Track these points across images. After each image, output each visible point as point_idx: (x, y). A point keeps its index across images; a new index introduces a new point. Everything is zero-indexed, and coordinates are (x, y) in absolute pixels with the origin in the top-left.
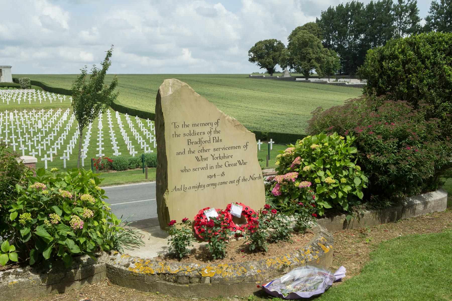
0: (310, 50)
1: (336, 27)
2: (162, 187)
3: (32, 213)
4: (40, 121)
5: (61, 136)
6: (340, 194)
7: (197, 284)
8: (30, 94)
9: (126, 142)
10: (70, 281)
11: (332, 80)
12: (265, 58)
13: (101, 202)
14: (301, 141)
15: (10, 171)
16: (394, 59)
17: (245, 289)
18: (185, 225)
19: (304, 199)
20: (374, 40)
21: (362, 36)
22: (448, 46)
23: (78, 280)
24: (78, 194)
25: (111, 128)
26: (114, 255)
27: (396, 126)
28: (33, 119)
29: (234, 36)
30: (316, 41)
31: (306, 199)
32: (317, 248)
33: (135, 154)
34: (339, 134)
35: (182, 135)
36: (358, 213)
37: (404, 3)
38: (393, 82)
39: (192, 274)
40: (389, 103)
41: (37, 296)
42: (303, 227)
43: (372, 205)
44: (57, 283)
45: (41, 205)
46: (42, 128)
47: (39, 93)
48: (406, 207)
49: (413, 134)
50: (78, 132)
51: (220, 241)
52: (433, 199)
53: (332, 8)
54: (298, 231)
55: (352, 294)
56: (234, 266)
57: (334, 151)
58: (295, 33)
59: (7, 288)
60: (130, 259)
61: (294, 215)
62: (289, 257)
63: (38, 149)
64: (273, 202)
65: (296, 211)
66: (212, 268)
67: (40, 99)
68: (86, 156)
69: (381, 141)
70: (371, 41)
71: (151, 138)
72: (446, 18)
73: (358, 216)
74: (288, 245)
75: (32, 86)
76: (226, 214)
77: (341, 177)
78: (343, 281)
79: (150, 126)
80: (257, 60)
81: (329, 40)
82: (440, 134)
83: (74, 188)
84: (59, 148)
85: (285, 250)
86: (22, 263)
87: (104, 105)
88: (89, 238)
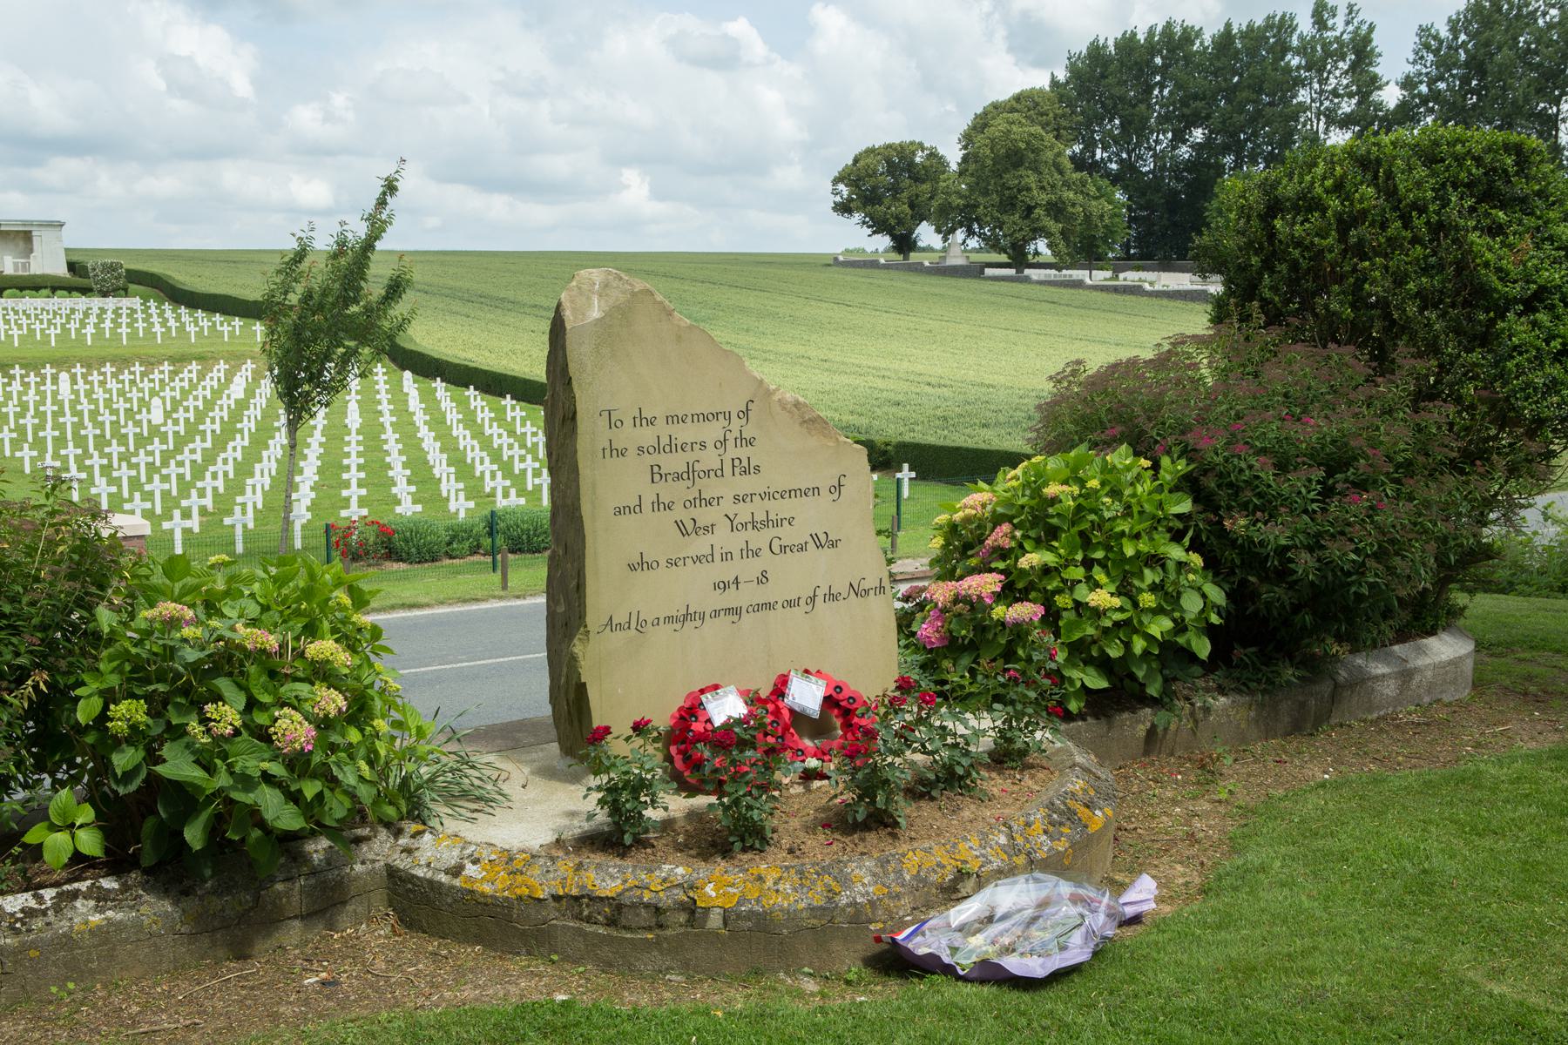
0: (1031, 179)
1: (1115, 105)
2: (566, 617)
3: (148, 698)
4: (156, 401)
5: (224, 450)
6: (1139, 645)
7: (682, 930)
8: (124, 311)
9: (436, 471)
10: (267, 919)
11: (1101, 276)
12: (887, 202)
13: (371, 665)
14: (1013, 473)
15: (78, 564)
16: (1310, 210)
17: (837, 946)
18: (639, 741)
19: (1020, 659)
20: (1235, 147)
21: (1198, 134)
22: (1482, 170)
23: (296, 917)
24: (297, 639)
25: (388, 425)
26: (413, 836)
27: (1315, 430)
28: (135, 395)
29: (787, 128)
30: (1052, 147)
31: (1029, 660)
32: (1063, 815)
33: (467, 510)
34: (1137, 454)
35: (632, 452)
36: (1192, 705)
37: (1333, 29)
38: (1309, 285)
39: (665, 900)
40: (1297, 353)
41: (165, 966)
42: (1019, 751)
43: (1238, 680)
44: (228, 927)
45: (179, 676)
46: (165, 424)
47: (153, 310)
48: (1343, 687)
49: (1369, 452)
50: (282, 438)
51: (754, 792)
52: (1428, 661)
53: (1101, 42)
54: (1002, 762)
55: (1179, 963)
56: (801, 873)
57: (1117, 506)
58: (982, 123)
59: (67, 941)
60: (463, 848)
61: (990, 709)
62: (975, 843)
63: (152, 493)
64: (923, 667)
65: (997, 698)
66: (730, 879)
67: (157, 329)
68: (309, 515)
69: (1268, 475)
70: (1226, 149)
71: (517, 459)
72: (1465, 80)
73: (1192, 714)
74: (973, 807)
75: (132, 287)
76: (770, 707)
77: (1140, 591)
78: (1147, 920)
79: (514, 419)
80: (858, 210)
81: (1090, 146)
82: (1455, 454)
83: (284, 622)
84: (221, 490)
85: (962, 822)
86: (116, 861)
87: (366, 351)
88: (333, 782)
